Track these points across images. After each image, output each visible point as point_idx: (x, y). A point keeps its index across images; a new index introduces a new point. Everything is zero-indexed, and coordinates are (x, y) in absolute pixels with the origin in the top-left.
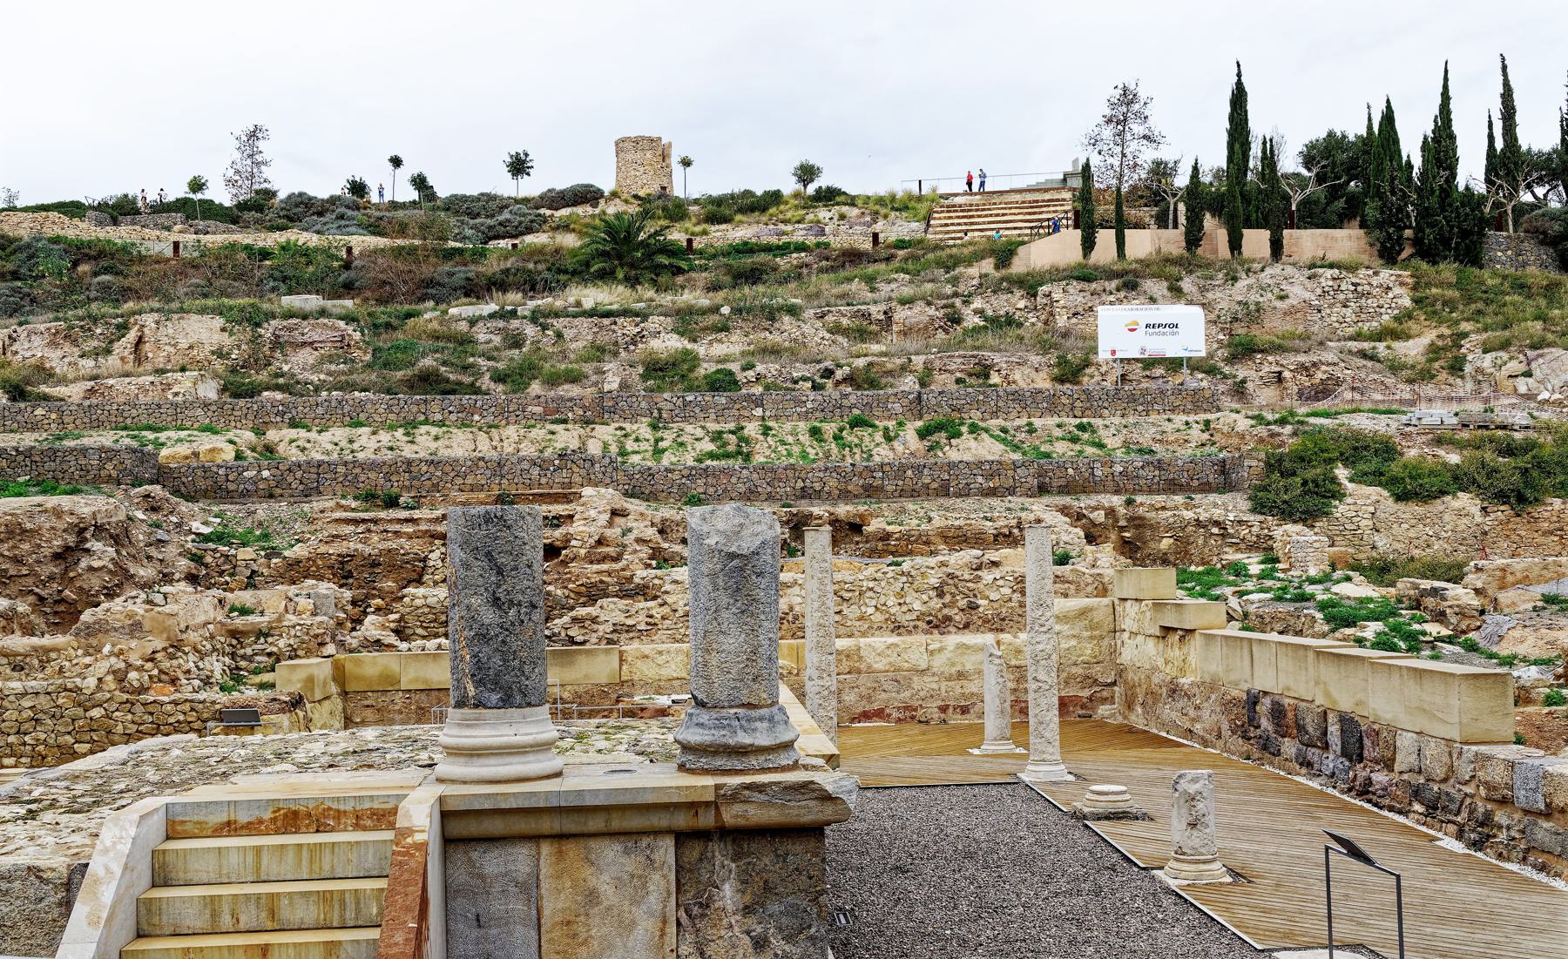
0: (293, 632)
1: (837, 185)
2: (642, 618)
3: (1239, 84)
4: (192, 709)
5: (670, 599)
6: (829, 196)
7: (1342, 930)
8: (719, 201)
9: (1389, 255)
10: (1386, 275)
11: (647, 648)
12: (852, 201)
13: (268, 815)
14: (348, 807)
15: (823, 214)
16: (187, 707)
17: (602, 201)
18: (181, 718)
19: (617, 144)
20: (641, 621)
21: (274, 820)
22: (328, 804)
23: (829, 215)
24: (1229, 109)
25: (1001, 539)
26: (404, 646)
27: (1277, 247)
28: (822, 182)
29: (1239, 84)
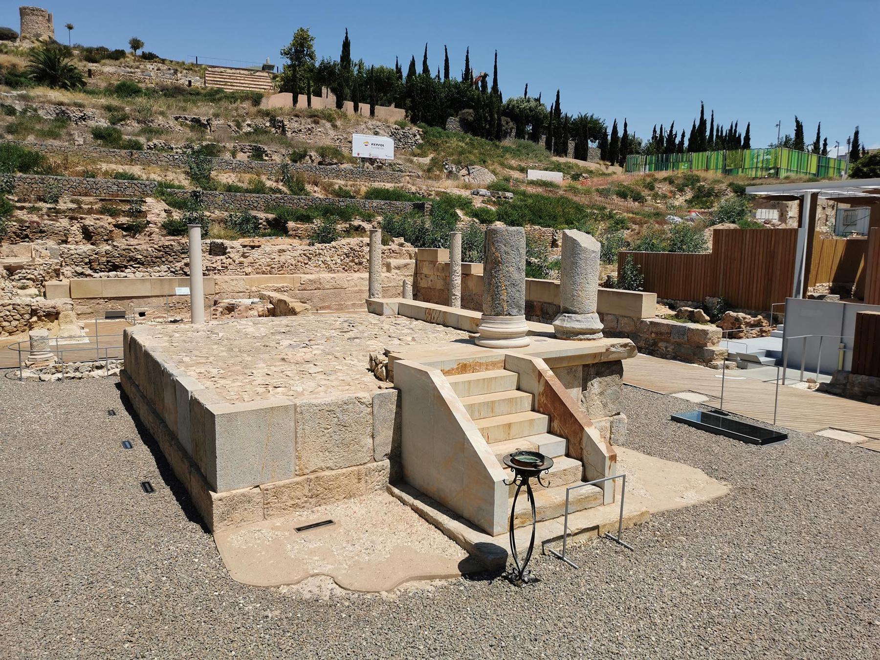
0: (42, 267)
1: (154, 52)
2: (219, 263)
3: (347, 38)
4: (14, 309)
5: (232, 255)
6: (149, 57)
7: (719, 395)
8: (90, 50)
9: (414, 121)
10: (415, 129)
11: (226, 278)
12: (163, 61)
13: (455, 367)
14: (483, 361)
15: (149, 66)
16: (10, 307)
17: (18, 40)
18: (8, 313)
19: (20, 9)
20: (218, 266)
21: (457, 368)
22: (477, 360)
23: (151, 67)
24: (95, 46)
25: (352, 231)
26: (96, 275)
27: (372, 112)
28: (146, 49)
29: (347, 38)
